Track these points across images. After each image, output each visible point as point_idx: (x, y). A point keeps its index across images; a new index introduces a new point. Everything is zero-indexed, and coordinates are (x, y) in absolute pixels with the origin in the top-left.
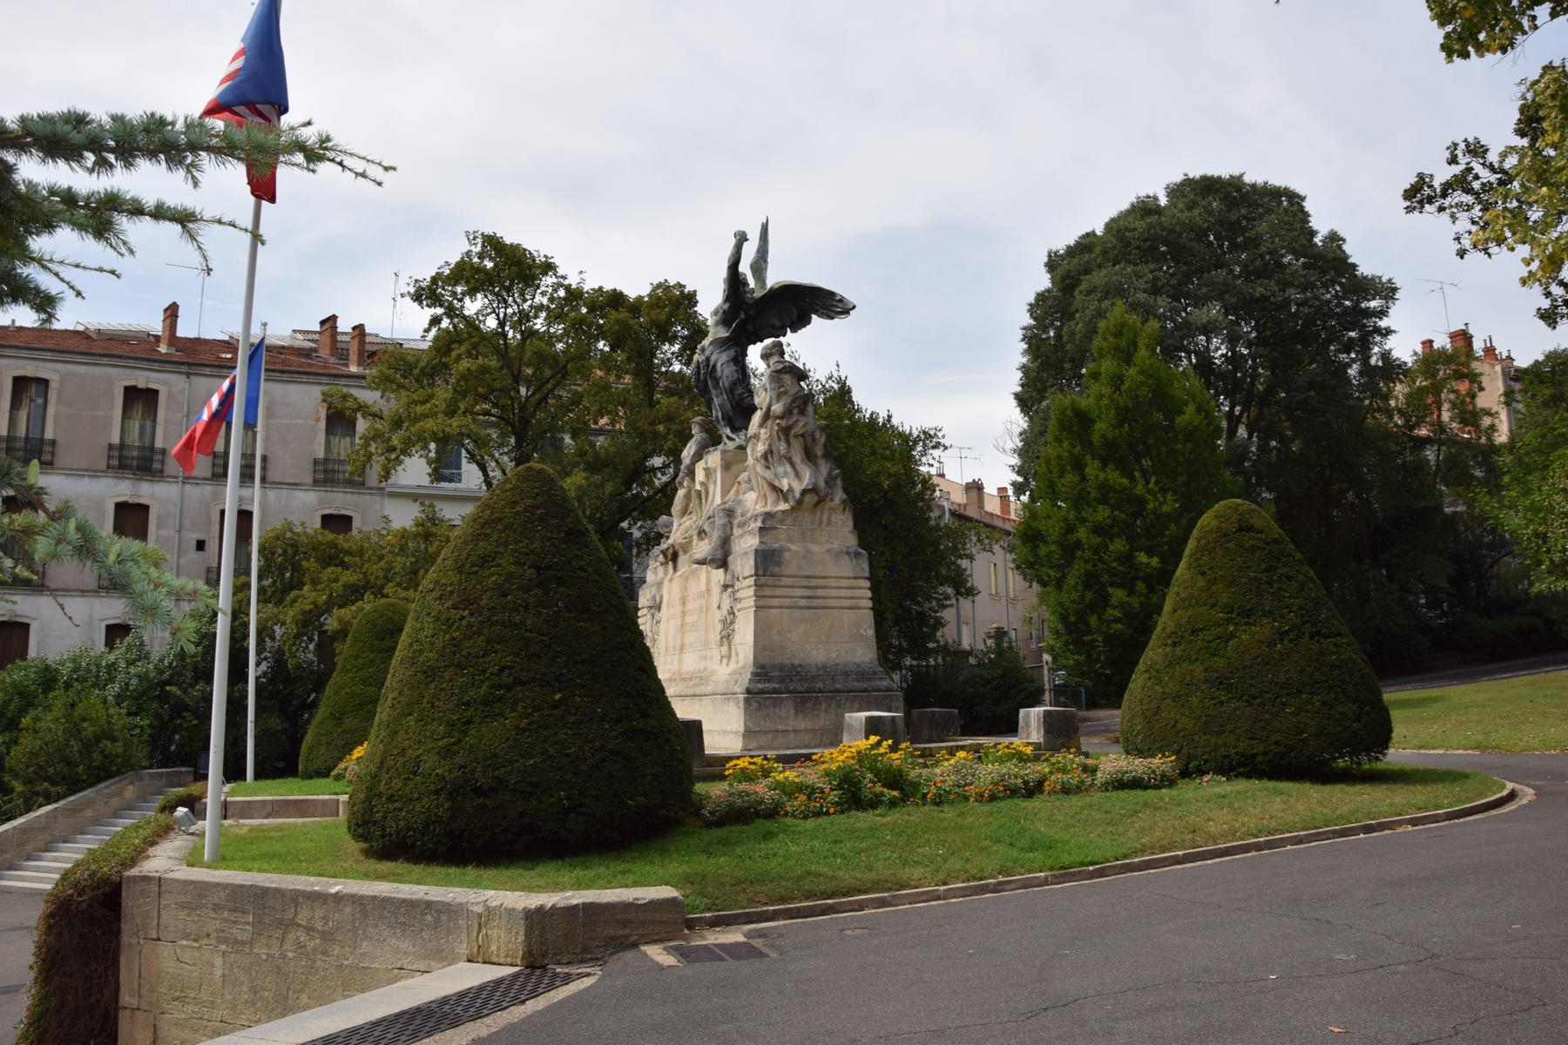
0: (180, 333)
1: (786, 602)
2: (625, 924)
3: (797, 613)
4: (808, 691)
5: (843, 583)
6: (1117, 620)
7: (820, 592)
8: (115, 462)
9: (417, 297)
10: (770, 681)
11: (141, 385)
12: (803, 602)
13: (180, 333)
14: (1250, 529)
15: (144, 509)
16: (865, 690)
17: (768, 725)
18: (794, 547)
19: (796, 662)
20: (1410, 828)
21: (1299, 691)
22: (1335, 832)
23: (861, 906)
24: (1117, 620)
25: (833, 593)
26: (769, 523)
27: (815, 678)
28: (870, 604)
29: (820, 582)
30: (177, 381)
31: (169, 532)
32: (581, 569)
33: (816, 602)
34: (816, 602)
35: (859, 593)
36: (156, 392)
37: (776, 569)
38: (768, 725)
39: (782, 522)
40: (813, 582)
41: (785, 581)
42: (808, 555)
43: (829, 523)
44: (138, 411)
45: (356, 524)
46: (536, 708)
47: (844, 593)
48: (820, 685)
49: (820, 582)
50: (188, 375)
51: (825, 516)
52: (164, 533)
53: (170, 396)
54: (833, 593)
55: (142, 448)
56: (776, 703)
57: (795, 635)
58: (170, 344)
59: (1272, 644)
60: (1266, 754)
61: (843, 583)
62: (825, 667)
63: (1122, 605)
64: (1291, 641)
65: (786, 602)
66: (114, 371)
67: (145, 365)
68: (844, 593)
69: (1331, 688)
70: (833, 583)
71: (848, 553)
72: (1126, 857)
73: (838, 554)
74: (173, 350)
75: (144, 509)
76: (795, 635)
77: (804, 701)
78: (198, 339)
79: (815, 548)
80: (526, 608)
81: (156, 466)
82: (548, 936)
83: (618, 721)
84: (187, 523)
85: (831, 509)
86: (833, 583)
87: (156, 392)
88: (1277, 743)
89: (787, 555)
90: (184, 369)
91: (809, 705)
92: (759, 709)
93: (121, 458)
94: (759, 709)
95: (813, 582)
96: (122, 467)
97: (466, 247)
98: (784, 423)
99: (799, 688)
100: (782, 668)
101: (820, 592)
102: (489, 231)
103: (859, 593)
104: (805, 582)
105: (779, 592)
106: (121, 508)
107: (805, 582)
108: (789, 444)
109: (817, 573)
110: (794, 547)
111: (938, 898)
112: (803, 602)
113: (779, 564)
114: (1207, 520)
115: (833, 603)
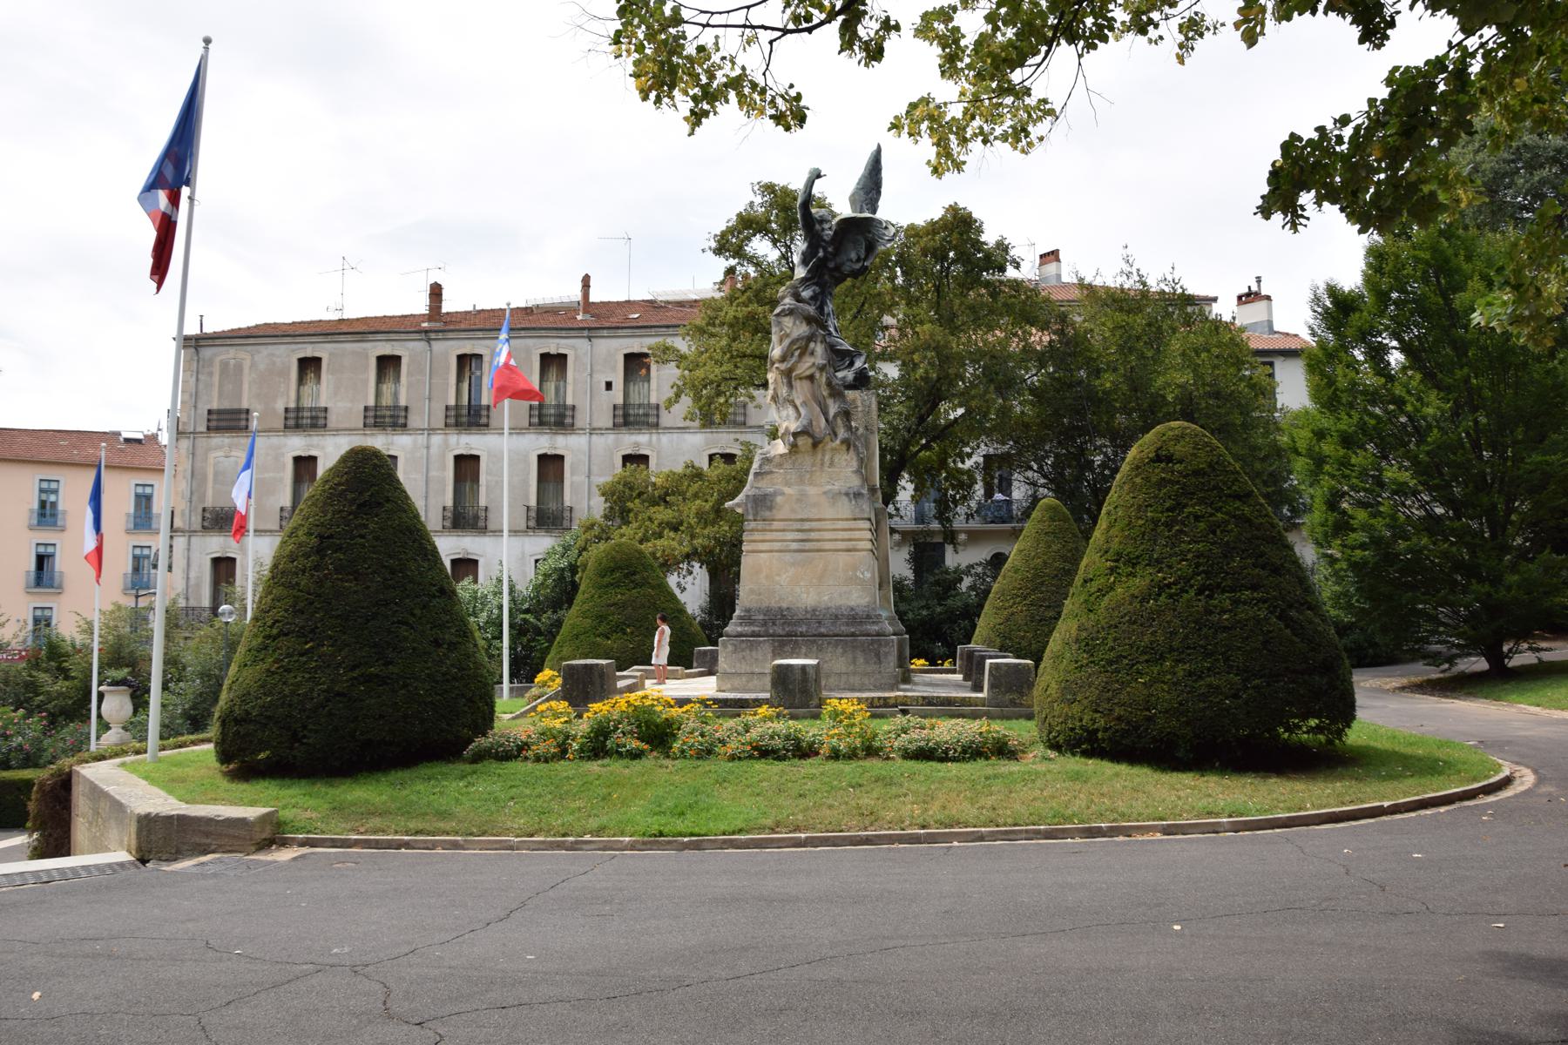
0: (593, 298)
1: (777, 546)
2: (207, 834)
3: (788, 556)
4: (788, 635)
5: (840, 525)
6: (1363, 546)
7: (813, 535)
8: (536, 420)
9: (719, 251)
10: (751, 624)
11: (553, 351)
12: (794, 546)
13: (593, 298)
14: (1169, 459)
15: (560, 458)
16: (853, 635)
17: (744, 668)
18: (787, 490)
19: (785, 605)
20: (1159, 836)
21: (1162, 657)
22: (1038, 832)
23: (434, 845)
24: (1363, 546)
25: (827, 535)
26: (766, 468)
27: (800, 622)
28: (869, 545)
29: (814, 525)
30: (582, 344)
31: (581, 478)
32: (362, 537)
33: (808, 545)
34: (808, 545)
35: (857, 534)
36: (565, 356)
37: (767, 514)
38: (744, 668)
39: (780, 465)
40: (807, 525)
41: (776, 525)
42: (802, 498)
43: (832, 464)
44: (553, 373)
45: (652, 462)
46: (289, 655)
47: (841, 535)
48: (804, 629)
49: (814, 525)
50: (590, 338)
51: (827, 457)
52: (576, 478)
53: (576, 357)
54: (827, 535)
55: (558, 406)
56: (752, 646)
57: (784, 579)
58: (585, 312)
59: (1144, 600)
60: (1106, 730)
61: (840, 525)
62: (814, 610)
63: (1365, 527)
64: (1171, 596)
65: (777, 546)
66: (530, 342)
67: (554, 333)
68: (841, 535)
69: (1208, 655)
70: (828, 525)
71: (847, 494)
72: (733, 833)
73: (834, 497)
74: (588, 317)
75: (560, 458)
76: (784, 579)
77: (782, 644)
78: (628, 302)
79: (812, 491)
80: (304, 572)
81: (568, 421)
82: (153, 837)
83: (354, 668)
84: (595, 469)
85: (833, 449)
86: (828, 525)
87: (565, 356)
88: (1119, 718)
89: (779, 499)
90: (586, 333)
91: (787, 648)
92: (735, 651)
93: (540, 416)
94: (735, 651)
95: (807, 525)
96: (541, 423)
97: (751, 197)
98: (783, 366)
99: (780, 631)
100: (768, 611)
101: (813, 535)
102: (766, 180)
103: (857, 534)
104: (798, 525)
105: (769, 536)
106: (543, 459)
107: (798, 525)
108: (790, 386)
109: (811, 516)
110: (787, 490)
111: (511, 848)
112: (794, 546)
113: (770, 508)
114: (1132, 453)
115: (828, 545)
